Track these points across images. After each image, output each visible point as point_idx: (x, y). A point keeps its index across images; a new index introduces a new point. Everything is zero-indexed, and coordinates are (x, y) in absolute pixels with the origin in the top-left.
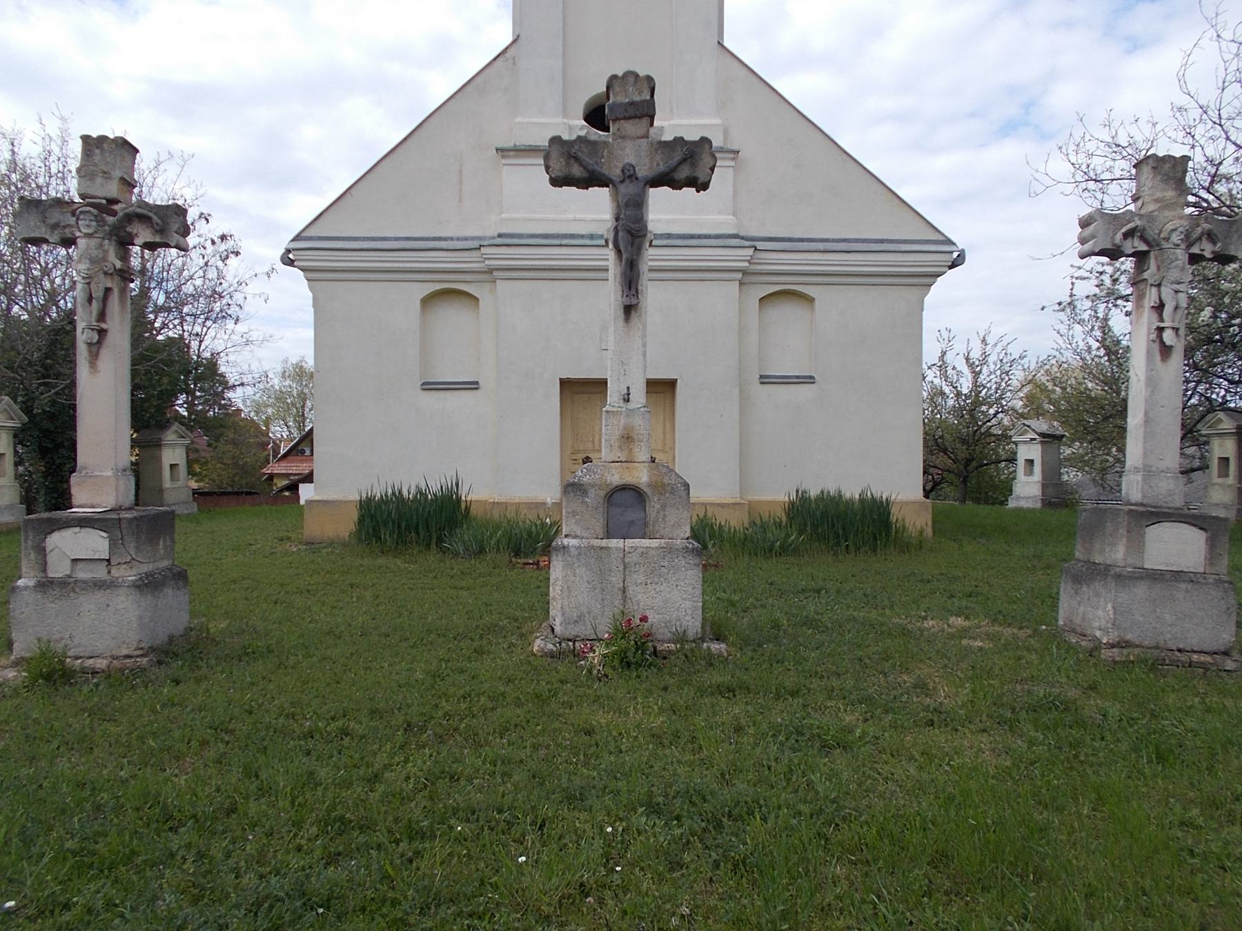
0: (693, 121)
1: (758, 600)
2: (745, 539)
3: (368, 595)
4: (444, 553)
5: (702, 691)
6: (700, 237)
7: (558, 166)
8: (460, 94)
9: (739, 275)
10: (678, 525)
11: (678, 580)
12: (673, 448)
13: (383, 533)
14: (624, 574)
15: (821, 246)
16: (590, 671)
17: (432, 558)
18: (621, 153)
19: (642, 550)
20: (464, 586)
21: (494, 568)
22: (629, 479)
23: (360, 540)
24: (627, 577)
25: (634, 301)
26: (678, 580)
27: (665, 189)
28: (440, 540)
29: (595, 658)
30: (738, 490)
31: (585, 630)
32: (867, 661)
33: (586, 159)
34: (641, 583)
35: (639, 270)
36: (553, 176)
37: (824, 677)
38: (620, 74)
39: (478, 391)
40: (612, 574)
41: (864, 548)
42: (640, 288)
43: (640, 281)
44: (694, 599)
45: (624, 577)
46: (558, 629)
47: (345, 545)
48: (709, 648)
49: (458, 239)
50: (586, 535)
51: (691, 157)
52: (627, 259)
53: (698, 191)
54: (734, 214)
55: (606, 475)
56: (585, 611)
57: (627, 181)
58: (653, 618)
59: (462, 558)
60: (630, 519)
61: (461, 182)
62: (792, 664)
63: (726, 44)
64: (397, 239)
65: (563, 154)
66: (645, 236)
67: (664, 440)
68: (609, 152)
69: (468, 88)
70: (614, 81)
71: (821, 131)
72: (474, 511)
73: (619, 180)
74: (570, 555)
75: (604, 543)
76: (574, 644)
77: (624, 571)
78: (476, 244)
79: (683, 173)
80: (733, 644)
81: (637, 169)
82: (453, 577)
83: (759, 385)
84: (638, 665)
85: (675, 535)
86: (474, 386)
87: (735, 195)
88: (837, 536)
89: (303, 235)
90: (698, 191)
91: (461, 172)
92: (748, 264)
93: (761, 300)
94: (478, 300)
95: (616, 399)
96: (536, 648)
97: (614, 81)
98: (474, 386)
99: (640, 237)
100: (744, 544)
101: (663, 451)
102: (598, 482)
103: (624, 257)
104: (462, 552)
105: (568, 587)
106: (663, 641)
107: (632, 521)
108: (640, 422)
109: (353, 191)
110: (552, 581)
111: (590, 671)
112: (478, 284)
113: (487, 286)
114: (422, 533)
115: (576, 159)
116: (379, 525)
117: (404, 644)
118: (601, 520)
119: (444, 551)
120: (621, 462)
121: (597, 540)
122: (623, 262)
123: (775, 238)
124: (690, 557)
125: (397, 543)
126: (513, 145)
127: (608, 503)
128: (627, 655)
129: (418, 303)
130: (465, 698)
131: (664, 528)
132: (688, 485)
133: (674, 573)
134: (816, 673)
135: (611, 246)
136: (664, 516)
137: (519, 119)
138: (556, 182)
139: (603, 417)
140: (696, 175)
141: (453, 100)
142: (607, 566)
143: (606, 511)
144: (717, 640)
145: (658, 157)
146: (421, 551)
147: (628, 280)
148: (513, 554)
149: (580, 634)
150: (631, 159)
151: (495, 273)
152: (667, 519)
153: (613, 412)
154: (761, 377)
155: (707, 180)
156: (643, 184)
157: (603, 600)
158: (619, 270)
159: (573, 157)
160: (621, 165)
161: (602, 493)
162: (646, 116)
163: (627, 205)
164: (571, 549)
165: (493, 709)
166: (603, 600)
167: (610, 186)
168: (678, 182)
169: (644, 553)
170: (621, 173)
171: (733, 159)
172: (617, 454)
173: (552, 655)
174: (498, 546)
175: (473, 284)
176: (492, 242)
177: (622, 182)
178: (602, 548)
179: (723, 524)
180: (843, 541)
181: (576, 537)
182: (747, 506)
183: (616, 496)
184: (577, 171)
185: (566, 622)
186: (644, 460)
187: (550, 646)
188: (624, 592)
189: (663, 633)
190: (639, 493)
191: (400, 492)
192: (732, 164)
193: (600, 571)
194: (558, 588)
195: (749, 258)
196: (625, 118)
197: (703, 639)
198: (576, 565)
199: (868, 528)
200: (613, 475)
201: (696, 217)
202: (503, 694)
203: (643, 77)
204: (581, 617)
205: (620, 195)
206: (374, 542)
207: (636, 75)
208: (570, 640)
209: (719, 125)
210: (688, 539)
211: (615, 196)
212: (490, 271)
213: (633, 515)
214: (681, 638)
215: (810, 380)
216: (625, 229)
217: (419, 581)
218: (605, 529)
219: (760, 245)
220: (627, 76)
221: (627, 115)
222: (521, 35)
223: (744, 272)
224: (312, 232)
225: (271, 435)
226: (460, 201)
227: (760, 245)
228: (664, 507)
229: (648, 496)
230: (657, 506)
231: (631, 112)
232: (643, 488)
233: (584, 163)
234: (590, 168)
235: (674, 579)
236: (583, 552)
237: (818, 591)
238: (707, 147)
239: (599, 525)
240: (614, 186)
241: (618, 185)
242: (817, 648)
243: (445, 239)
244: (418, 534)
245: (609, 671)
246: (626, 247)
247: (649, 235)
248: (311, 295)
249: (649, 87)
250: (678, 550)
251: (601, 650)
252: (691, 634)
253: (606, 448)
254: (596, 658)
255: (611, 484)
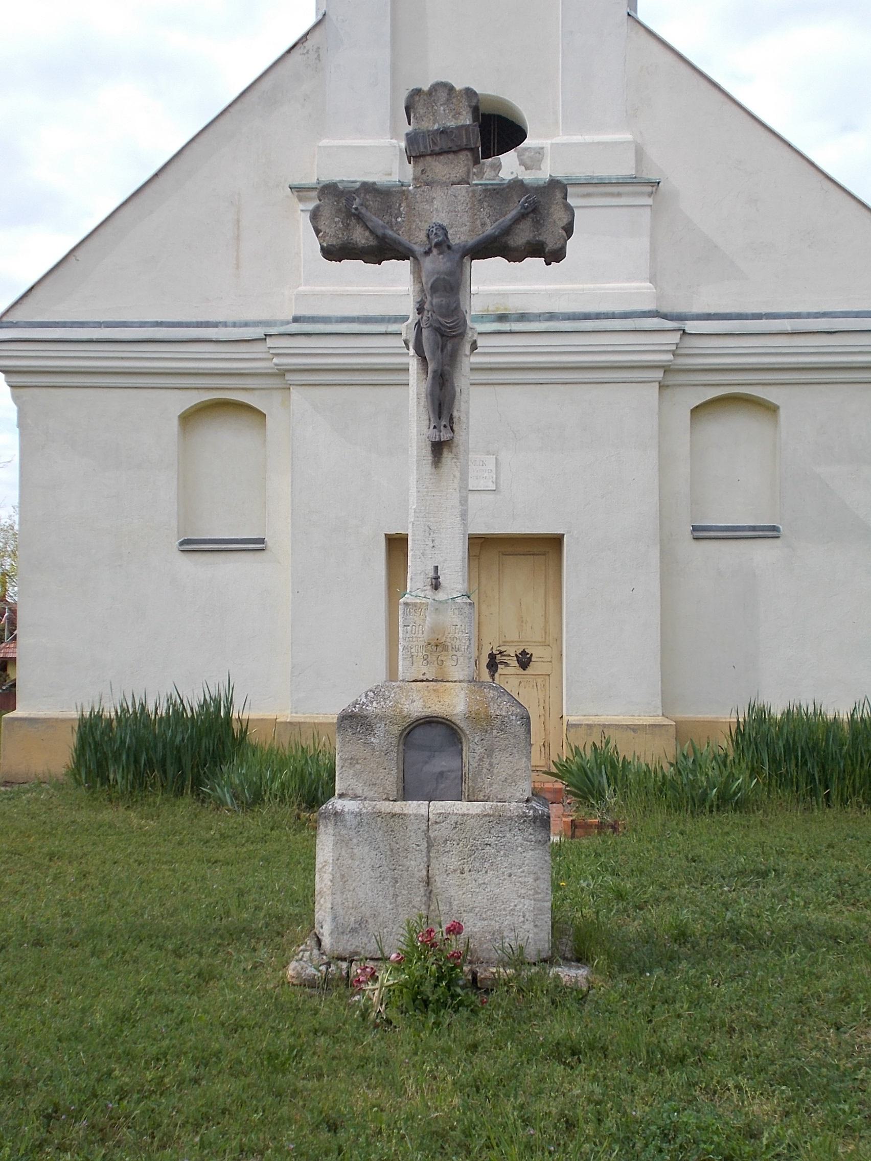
0: (588, 138)
1: (665, 889)
2: (663, 784)
3: (72, 870)
4: (203, 801)
5: (530, 1052)
6: (598, 316)
7: (334, 234)
8: (238, 107)
9: (659, 374)
10: (510, 780)
11: (512, 865)
12: (559, 640)
13: (111, 770)
14: (429, 857)
15: (787, 325)
16: (364, 1015)
17: (185, 806)
18: (427, 207)
19: (454, 818)
20: (221, 858)
21: (272, 829)
22: (436, 708)
23: (78, 783)
24: (433, 861)
25: (445, 435)
26: (512, 865)
27: (498, 262)
28: (197, 783)
29: (374, 992)
30: (659, 704)
31: (365, 944)
32: (815, 1003)
33: (374, 218)
34: (455, 871)
35: (453, 388)
36: (325, 245)
37: (734, 1030)
38: (426, 88)
39: (264, 552)
40: (409, 856)
41: (855, 799)
42: (455, 414)
43: (456, 402)
44: (536, 896)
45: (429, 861)
46: (327, 941)
47: (59, 786)
48: (557, 977)
49: (234, 325)
50: (371, 794)
51: (534, 211)
52: (435, 372)
53: (548, 264)
54: (652, 279)
55: (402, 701)
56: (368, 914)
57: (435, 251)
58: (472, 926)
59: (229, 810)
60: (438, 769)
61: (238, 238)
62: (686, 1006)
63: (641, 16)
64: (142, 325)
65: (339, 210)
66: (462, 335)
67: (545, 627)
68: (408, 206)
69: (253, 96)
70: (417, 98)
71: (790, 146)
72: (254, 736)
73: (422, 250)
74: (345, 826)
75: (398, 807)
76: (349, 967)
77: (429, 852)
78: (259, 332)
79: (522, 236)
80: (597, 970)
81: (450, 232)
82: (207, 842)
83: (693, 542)
84: (441, 1005)
85: (509, 795)
86: (257, 545)
87: (654, 250)
88: (811, 779)
89: (5, 319)
90: (548, 264)
91: (238, 221)
92: (670, 357)
93: (695, 411)
94: (265, 415)
95: (420, 585)
96: (291, 972)
97: (417, 98)
98: (257, 545)
99: (454, 336)
100: (661, 792)
101: (545, 644)
102: (390, 712)
103: (431, 368)
104: (229, 800)
105: (343, 876)
106: (489, 963)
107: (441, 774)
108: (456, 620)
109: (79, 254)
110: (318, 866)
111: (364, 1015)
112: (263, 392)
113: (277, 396)
114: (171, 770)
115: (359, 218)
116: (106, 759)
117: (93, 961)
118: (395, 771)
119: (202, 799)
120: (427, 680)
121: (387, 803)
122: (430, 375)
123: (715, 314)
124: (530, 831)
125: (133, 787)
126: (315, 181)
127: (404, 745)
128: (422, 989)
129: (175, 422)
130: (158, 1060)
131: (491, 785)
132: (529, 718)
133: (505, 855)
134: (723, 1024)
135: (412, 351)
136: (491, 764)
137: (325, 142)
138: (332, 253)
139: (401, 612)
140: (541, 238)
141: (227, 116)
142: (402, 844)
143: (401, 755)
144: (578, 960)
145: (484, 213)
146: (168, 800)
147: (437, 403)
148: (304, 805)
149: (359, 950)
150: (442, 218)
151: (289, 377)
152: (495, 771)
153: (415, 605)
154: (695, 529)
155: (559, 245)
156: (458, 256)
157: (396, 896)
158: (425, 386)
159: (354, 215)
160: (426, 226)
161: (396, 730)
162: (466, 149)
163: (434, 289)
164: (347, 817)
165: (196, 1081)
166: (396, 896)
167: (411, 258)
168: (516, 249)
169: (459, 823)
170: (425, 239)
171: (650, 194)
172: (422, 669)
173: (311, 983)
174: (283, 793)
175: (257, 392)
176: (282, 329)
177: (427, 253)
178: (394, 815)
179: (629, 759)
180: (821, 788)
181: (355, 797)
182: (673, 731)
183: (418, 733)
184: (360, 237)
185: (339, 930)
186: (461, 678)
187: (311, 971)
188: (428, 884)
189: (486, 949)
190: (453, 729)
191: (143, 707)
192: (649, 201)
193: (392, 850)
194: (327, 877)
195: (674, 348)
196: (434, 154)
197: (548, 961)
198: (355, 841)
199: (862, 766)
200: (413, 701)
201: (592, 286)
202: (217, 1054)
203: (461, 91)
204: (362, 923)
205: (423, 274)
206: (98, 785)
207: (450, 89)
208: (344, 959)
209: (629, 142)
210: (528, 801)
211: (417, 272)
212: (282, 373)
213: (443, 763)
214: (518, 960)
215: (770, 532)
216: (431, 326)
217: (155, 850)
218: (401, 785)
219: (691, 326)
220: (436, 90)
221: (437, 149)
222: (331, 14)
223: (667, 369)
224: (18, 316)
225: (9, 599)
226: (238, 267)
227: (691, 326)
228: (490, 752)
229: (465, 735)
230: (479, 750)
231: (443, 143)
232: (458, 722)
233: (370, 224)
234: (380, 232)
235: (506, 864)
236: (365, 821)
237: (764, 874)
238: (559, 195)
239: (390, 779)
240: (416, 258)
241: (421, 259)
242: (733, 979)
243: (215, 325)
244: (165, 772)
245: (394, 1014)
246: (433, 354)
247: (469, 333)
248: (15, 408)
249: (470, 106)
250: (511, 818)
251: (386, 978)
252: (531, 954)
253: (404, 659)
254: (377, 992)
255: (409, 716)
